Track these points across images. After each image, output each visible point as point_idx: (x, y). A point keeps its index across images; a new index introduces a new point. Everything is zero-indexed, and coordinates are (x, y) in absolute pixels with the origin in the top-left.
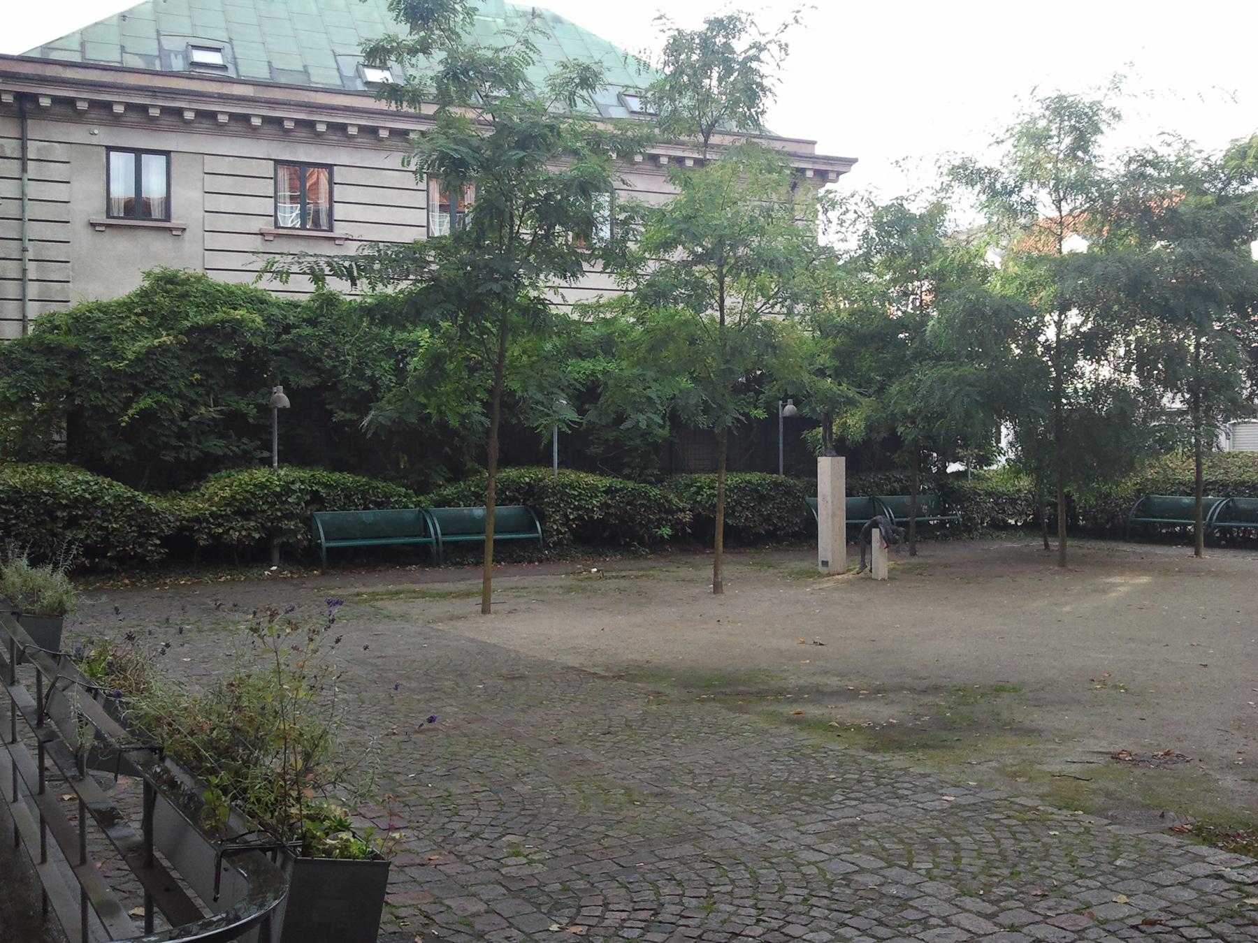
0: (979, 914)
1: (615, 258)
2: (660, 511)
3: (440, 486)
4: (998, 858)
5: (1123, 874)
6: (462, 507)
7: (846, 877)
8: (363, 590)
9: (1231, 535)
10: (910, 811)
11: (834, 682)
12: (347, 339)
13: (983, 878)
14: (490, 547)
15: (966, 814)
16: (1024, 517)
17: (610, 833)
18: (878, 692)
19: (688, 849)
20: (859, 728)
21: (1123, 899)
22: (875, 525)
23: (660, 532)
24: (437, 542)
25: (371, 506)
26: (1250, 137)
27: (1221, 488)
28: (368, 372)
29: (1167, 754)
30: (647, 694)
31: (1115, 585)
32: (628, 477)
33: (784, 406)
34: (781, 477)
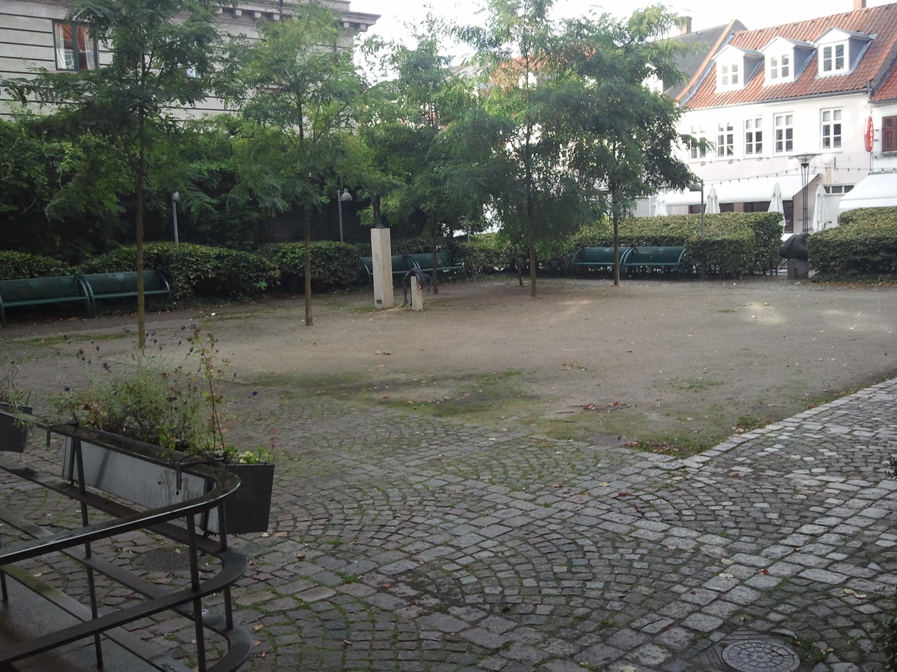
0: (525, 500)
1: (226, 90)
2: (257, 270)
3: (88, 258)
4: (529, 469)
5: (603, 471)
6: (107, 273)
7: (441, 488)
8: (39, 337)
9: (635, 271)
10: (471, 448)
11: (403, 377)
12: (4, 149)
13: (523, 481)
14: (142, 301)
15: (506, 447)
16: (505, 265)
17: (283, 478)
18: (432, 381)
19: (337, 483)
20: (426, 404)
21: (606, 484)
22: (413, 274)
23: (258, 286)
24: (91, 300)
25: (36, 275)
26: (644, 9)
27: (628, 241)
28: (25, 174)
29: (616, 404)
30: (279, 394)
31: (569, 306)
32: (230, 247)
33: (341, 194)
34: (342, 244)
